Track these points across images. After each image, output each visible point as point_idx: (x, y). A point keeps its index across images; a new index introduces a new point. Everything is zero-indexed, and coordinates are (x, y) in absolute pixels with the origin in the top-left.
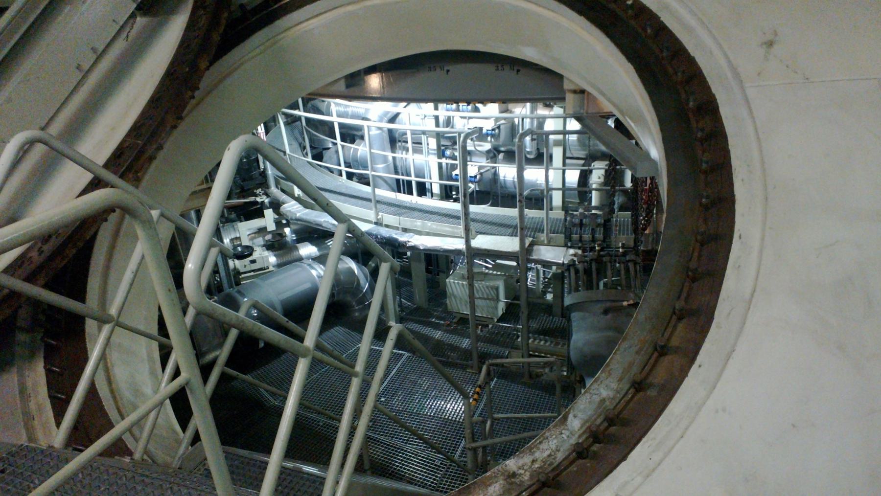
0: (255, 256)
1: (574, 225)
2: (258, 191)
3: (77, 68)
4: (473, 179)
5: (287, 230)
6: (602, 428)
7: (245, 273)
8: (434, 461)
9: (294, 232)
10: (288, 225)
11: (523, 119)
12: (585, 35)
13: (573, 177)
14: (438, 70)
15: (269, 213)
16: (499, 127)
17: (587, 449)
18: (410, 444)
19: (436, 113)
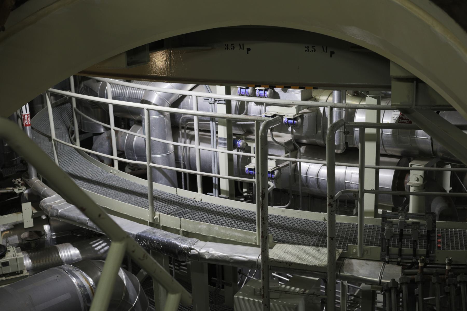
9: (52, 229)
10: (47, 222)
14: (237, 48)
15: (27, 207)
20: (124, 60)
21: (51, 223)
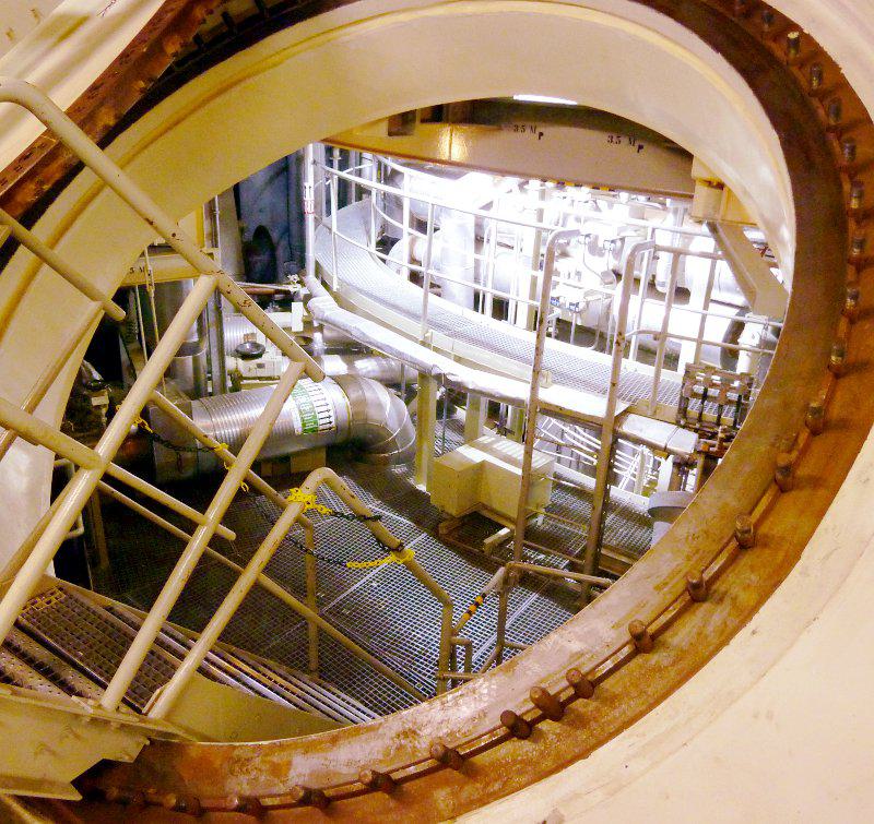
0: (264, 359)
1: (695, 395)
2: (291, 277)
3: (8, 34)
4: (572, 307)
5: (317, 336)
6: (563, 697)
7: (249, 379)
8: (415, 683)
9: (325, 340)
10: (321, 329)
11: (654, 230)
12: (695, 64)
13: (717, 332)
14: (528, 131)
15: (297, 306)
16: (623, 240)
17: (531, 725)
18: (390, 652)
19: (542, 204)
20: (383, 128)
21: (325, 331)
